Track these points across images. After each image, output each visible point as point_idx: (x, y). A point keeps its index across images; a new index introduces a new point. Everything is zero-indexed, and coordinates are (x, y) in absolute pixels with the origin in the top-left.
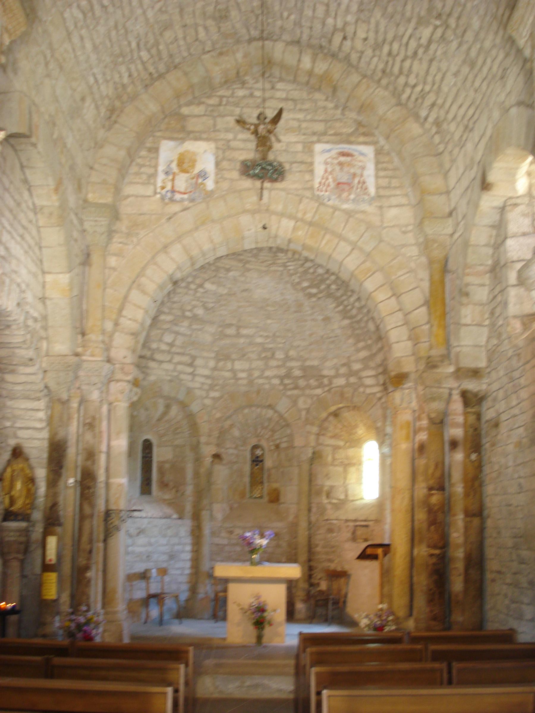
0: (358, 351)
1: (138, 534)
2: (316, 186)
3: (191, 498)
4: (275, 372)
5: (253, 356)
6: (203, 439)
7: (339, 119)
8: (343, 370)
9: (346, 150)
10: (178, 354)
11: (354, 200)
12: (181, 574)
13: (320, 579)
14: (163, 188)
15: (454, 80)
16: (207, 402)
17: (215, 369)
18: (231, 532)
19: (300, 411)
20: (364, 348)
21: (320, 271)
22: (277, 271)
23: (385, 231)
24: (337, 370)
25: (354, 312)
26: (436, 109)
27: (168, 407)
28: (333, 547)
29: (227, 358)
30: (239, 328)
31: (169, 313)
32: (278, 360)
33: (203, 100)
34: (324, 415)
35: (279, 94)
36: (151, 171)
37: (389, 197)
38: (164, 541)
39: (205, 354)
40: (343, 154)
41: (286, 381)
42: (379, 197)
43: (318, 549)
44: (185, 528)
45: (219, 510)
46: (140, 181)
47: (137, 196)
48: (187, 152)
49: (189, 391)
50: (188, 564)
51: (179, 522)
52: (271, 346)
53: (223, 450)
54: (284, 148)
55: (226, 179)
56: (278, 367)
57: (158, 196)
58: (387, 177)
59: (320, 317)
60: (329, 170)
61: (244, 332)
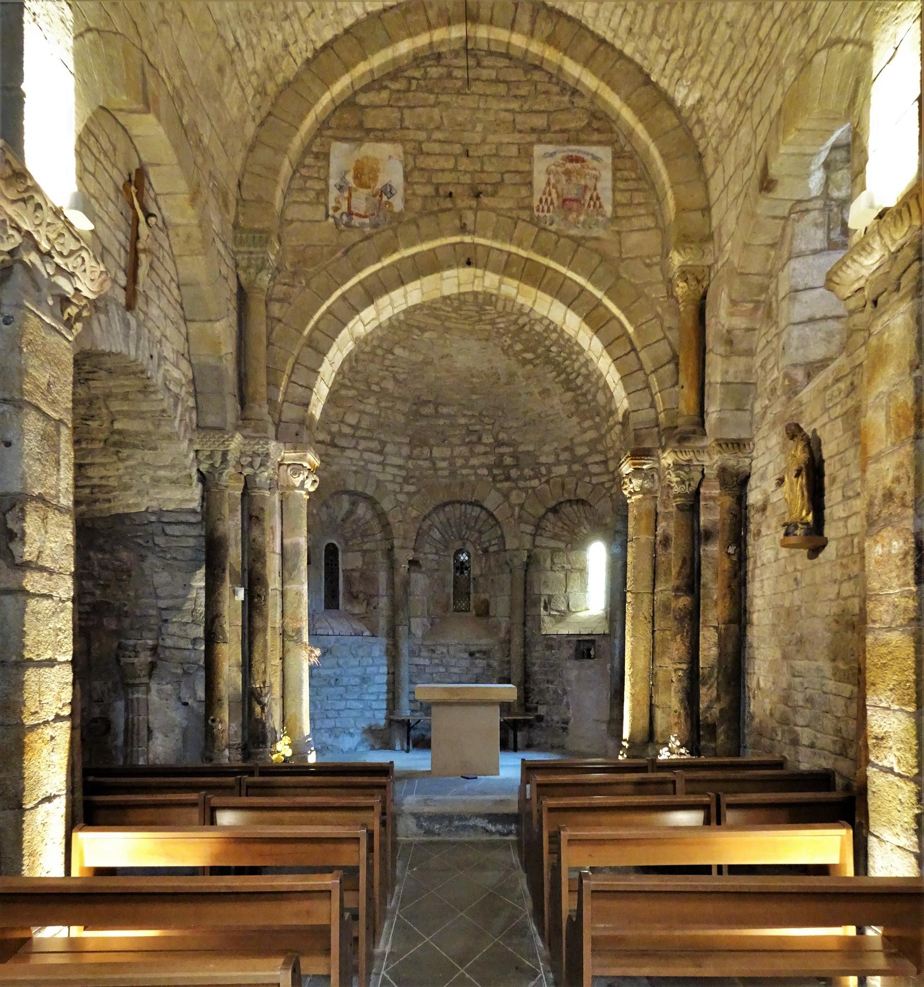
0: (584, 431)
2: (536, 203)
3: (385, 613)
4: (483, 460)
5: (455, 441)
6: (397, 543)
7: (568, 109)
8: (565, 456)
9: (574, 154)
10: (364, 438)
11: (584, 223)
14: (336, 209)
15: (729, 32)
16: (402, 498)
17: (410, 457)
18: (433, 651)
19: (512, 507)
20: (590, 428)
21: (538, 328)
24: (558, 455)
25: (579, 381)
26: (700, 84)
27: (354, 504)
29: (424, 443)
30: (437, 405)
31: (353, 388)
32: (486, 445)
35: (485, 74)
36: (319, 186)
37: (629, 218)
38: (355, 662)
39: (398, 439)
40: (571, 159)
41: (496, 472)
42: (615, 218)
43: (536, 668)
45: (418, 626)
47: (302, 221)
50: (385, 688)
51: (372, 640)
52: (477, 428)
53: (421, 555)
54: (494, 151)
56: (485, 453)
57: (331, 220)
58: (627, 190)
59: (536, 391)
60: (552, 181)
61: (444, 410)
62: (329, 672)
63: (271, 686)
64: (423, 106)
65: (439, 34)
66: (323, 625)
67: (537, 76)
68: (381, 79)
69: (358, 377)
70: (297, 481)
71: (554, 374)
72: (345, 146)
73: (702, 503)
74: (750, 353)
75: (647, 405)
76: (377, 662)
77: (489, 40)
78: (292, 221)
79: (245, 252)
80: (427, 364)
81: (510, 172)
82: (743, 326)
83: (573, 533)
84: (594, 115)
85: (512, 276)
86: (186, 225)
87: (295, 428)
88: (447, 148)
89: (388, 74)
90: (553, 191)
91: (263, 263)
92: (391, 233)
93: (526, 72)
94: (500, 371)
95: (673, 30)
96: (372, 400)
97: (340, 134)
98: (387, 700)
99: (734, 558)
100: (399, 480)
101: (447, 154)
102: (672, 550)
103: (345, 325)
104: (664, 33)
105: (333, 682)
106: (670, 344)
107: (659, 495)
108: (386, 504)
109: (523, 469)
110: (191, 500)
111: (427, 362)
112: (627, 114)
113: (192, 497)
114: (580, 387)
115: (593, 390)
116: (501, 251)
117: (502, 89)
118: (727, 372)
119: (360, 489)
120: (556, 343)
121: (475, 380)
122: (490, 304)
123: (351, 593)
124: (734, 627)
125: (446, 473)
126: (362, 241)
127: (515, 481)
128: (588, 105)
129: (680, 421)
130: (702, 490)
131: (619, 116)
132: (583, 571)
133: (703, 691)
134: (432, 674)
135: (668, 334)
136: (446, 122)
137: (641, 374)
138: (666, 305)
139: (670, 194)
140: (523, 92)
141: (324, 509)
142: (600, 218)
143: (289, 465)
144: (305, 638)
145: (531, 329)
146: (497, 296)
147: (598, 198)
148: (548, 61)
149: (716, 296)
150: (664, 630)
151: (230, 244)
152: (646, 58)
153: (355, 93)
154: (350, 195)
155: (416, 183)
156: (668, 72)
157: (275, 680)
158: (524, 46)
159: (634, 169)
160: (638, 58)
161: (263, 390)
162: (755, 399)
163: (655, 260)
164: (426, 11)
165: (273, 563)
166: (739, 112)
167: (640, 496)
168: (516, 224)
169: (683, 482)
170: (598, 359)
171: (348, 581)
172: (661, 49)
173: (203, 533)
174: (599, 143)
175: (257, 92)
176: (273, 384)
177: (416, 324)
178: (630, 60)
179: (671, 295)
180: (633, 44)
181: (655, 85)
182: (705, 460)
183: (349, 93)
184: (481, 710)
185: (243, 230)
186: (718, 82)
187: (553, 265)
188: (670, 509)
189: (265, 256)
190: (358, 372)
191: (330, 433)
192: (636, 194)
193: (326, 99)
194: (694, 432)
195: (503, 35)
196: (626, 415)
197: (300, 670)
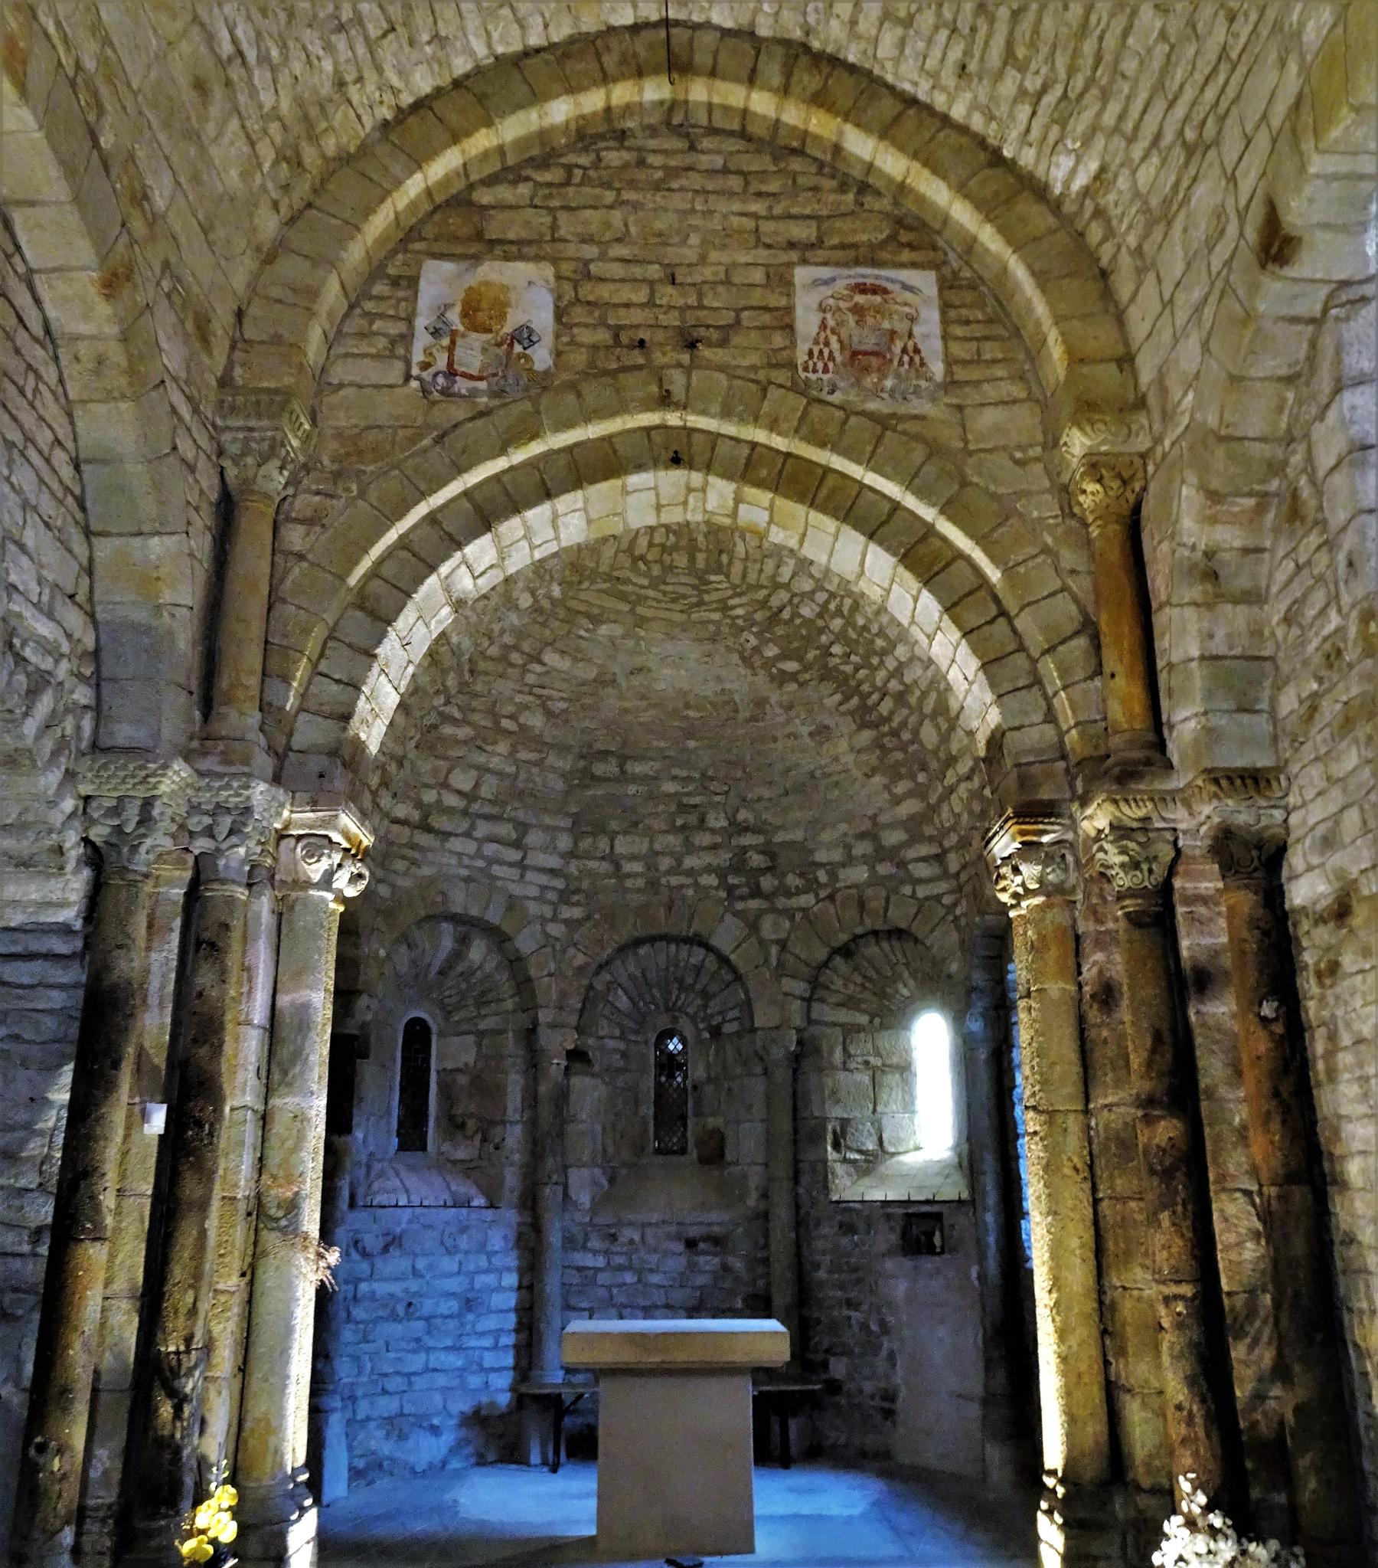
0: (897, 801)
1: (386, 1249)
4: (708, 859)
5: (658, 824)
6: (544, 1016)
8: (862, 848)
9: (868, 281)
10: (487, 817)
11: (892, 393)
12: (495, 1347)
13: (827, 1351)
14: (425, 366)
16: (556, 930)
17: (572, 855)
18: (613, 1238)
19: (762, 943)
20: (909, 794)
21: (806, 611)
22: (709, 622)
23: (970, 461)
24: (848, 848)
25: (886, 707)
26: (1100, 142)
27: (463, 941)
28: (856, 1270)
29: (599, 829)
30: (623, 759)
31: (465, 722)
32: (713, 831)
33: (529, 172)
34: (822, 954)
36: (396, 329)
37: (977, 384)
38: (449, 1264)
39: (548, 820)
40: (862, 289)
41: (732, 880)
42: (951, 384)
43: (822, 1274)
44: (499, 1233)
45: (583, 1183)
46: (374, 351)
47: (360, 387)
48: (487, 284)
49: (513, 904)
50: (511, 1320)
51: (489, 1215)
52: (697, 800)
53: (591, 1041)
55: (580, 345)
56: (714, 847)
57: (414, 384)
59: (805, 730)
60: (831, 323)
61: (637, 768)
62: (395, 1288)
63: (208, 1348)
64: (595, 208)
65: (622, 93)
66: (389, 1185)
67: (796, 164)
68: (520, 166)
69: (475, 704)
70: (315, 870)
71: (838, 697)
72: (448, 267)
73: (1180, 910)
74: (1254, 597)
75: (1038, 717)
76: (497, 1261)
77: (710, 107)
78: (341, 386)
79: (238, 429)
80: (604, 684)
81: (753, 308)
82: (1238, 543)
83: (882, 995)
84: (900, 222)
85: (759, 484)
86: (93, 337)
87: (316, 763)
88: (637, 271)
89: (532, 159)
90: (833, 339)
91: (272, 448)
92: (527, 406)
93: (776, 159)
94: (737, 698)
95: (1045, 50)
96: (502, 747)
97: (437, 248)
98: (516, 1347)
99: (1279, 1029)
100: (552, 896)
101: (635, 280)
102: (1124, 1013)
103: (433, 568)
104: (1028, 60)
105: (401, 1310)
106: (1076, 600)
107: (1080, 897)
108: (525, 942)
109: (784, 875)
110: (62, 904)
111: (605, 681)
112: (962, 214)
113: (66, 894)
114: (888, 719)
115: (913, 720)
116: (737, 440)
117: (735, 183)
118: (1211, 636)
119: (474, 912)
120: (841, 637)
121: (691, 713)
122: (719, 570)
123: (451, 1118)
124: (1300, 1195)
125: (640, 882)
126: (471, 419)
127: (769, 897)
128: (889, 208)
129: (1115, 741)
130: (1177, 883)
131: (946, 220)
132: (905, 1069)
133: (1238, 1352)
134: (609, 1288)
135: (1070, 582)
136: (633, 230)
137: (1020, 659)
138: (1060, 530)
139: (1053, 336)
140: (773, 186)
141: (403, 949)
142: (923, 384)
143: (300, 838)
144: (311, 1222)
145: (795, 615)
146: (733, 529)
147: (917, 351)
148: (817, 138)
149: (1167, 498)
150: (1124, 1200)
151: (208, 410)
152: (992, 118)
153: (471, 187)
154: (453, 342)
155: (577, 325)
156: (1035, 133)
157: (226, 1332)
158: (772, 114)
159: (980, 304)
160: (977, 123)
161: (253, 682)
162: (1278, 688)
163: (1031, 453)
164: (598, 56)
165: (244, 1052)
166: (1187, 164)
167: (1039, 900)
168: (765, 390)
169: (1136, 865)
170: (931, 638)
171: (447, 1094)
172: (1022, 92)
173: (84, 978)
174: (914, 265)
175: (280, 158)
176: (273, 671)
177: (582, 608)
178: (963, 129)
179: (1067, 506)
180: (968, 95)
181: (1010, 165)
182: (1180, 817)
183: (459, 185)
184: (713, 1388)
185: (237, 390)
186: (1137, 128)
187: (838, 463)
188: (1111, 925)
189: (279, 435)
190: (475, 695)
191: (419, 805)
192: (988, 345)
193: (414, 186)
194: (1148, 762)
195: (734, 95)
196: (996, 741)
197: (290, 1301)
